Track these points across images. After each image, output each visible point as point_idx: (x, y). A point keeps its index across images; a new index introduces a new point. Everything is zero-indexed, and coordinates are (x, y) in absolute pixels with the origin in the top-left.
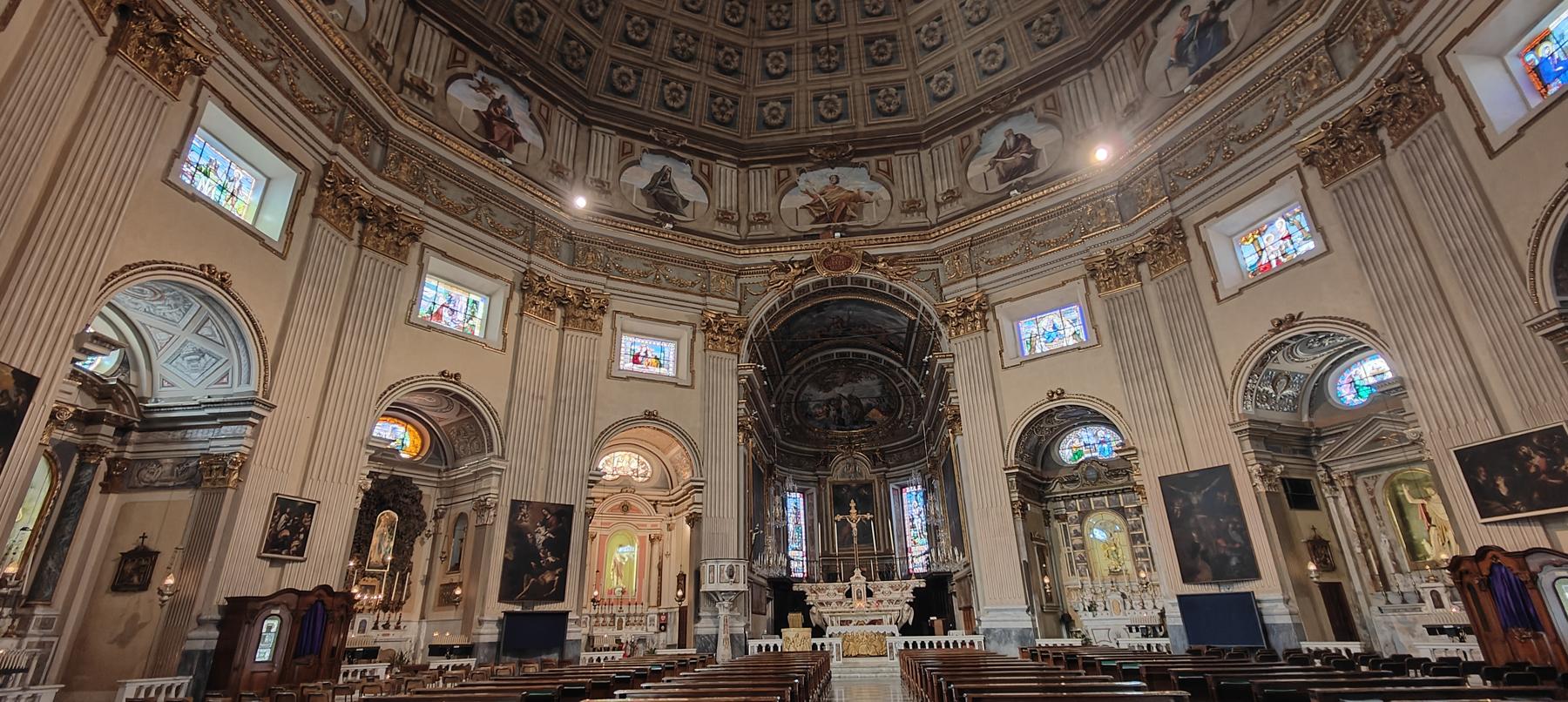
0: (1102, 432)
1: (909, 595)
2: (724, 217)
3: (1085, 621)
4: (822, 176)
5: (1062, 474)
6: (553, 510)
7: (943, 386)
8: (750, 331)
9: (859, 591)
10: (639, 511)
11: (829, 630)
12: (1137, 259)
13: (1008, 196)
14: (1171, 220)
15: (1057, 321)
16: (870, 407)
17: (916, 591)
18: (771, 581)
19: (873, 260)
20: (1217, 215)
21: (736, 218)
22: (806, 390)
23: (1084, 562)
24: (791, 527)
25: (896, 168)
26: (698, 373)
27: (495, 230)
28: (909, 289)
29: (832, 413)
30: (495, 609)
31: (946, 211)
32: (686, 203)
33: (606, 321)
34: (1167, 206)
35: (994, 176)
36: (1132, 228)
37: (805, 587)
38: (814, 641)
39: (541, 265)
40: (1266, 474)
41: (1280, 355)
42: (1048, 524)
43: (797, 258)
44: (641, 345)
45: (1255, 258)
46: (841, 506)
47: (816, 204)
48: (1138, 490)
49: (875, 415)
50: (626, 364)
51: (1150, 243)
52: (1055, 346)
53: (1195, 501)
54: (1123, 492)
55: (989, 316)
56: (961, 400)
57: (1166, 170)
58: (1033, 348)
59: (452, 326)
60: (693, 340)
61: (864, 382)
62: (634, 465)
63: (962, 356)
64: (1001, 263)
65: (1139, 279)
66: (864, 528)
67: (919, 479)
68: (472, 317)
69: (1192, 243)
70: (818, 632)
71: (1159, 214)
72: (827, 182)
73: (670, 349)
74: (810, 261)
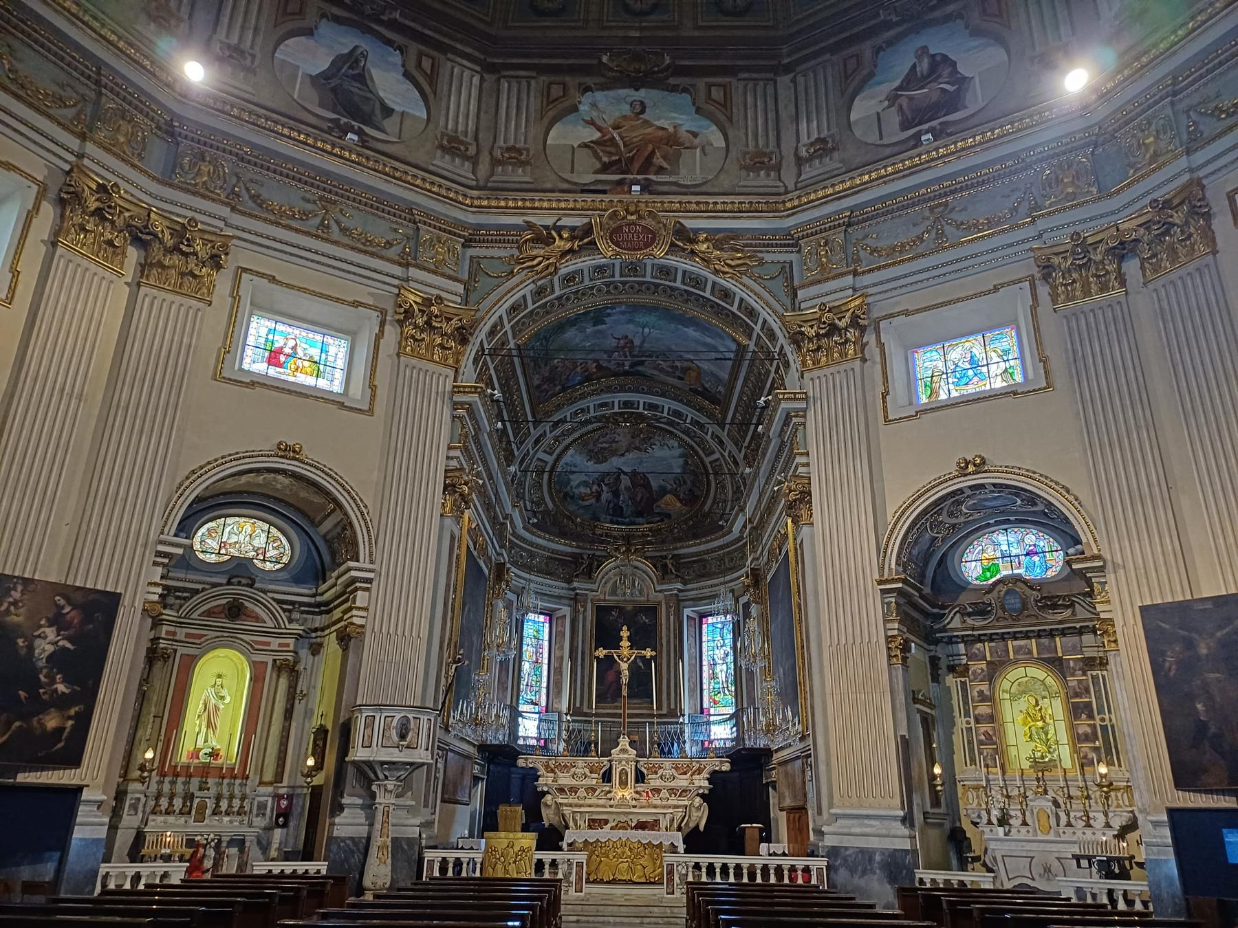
0: (1032, 538)
1: (702, 783)
2: (452, 146)
3: (989, 838)
4: (619, 100)
5: (964, 599)
7: (788, 450)
8: (481, 334)
9: (623, 773)
10: (257, 618)
11: (569, 836)
12: (1122, 250)
13: (918, 143)
14: (1190, 183)
15: (978, 351)
16: (663, 491)
17: (714, 777)
18: (483, 748)
21: (472, 151)
22: (567, 458)
23: (992, 745)
24: (526, 667)
25: (737, 99)
26: (382, 394)
28: (744, 290)
32: (388, 111)
33: (222, 282)
36: (1116, 203)
37: (536, 761)
38: (539, 855)
39: (102, 164)
42: (936, 678)
44: (286, 335)
47: (605, 143)
48: (1101, 628)
49: (670, 503)
50: (254, 363)
51: (1146, 225)
54: (1063, 633)
55: (870, 338)
56: (814, 469)
57: (1181, 106)
60: (379, 336)
61: (658, 452)
62: (260, 541)
63: (819, 399)
64: (895, 255)
65: (1123, 283)
66: (640, 676)
67: (729, 603)
70: (550, 838)
71: (1169, 178)
72: (626, 110)
73: (338, 350)
74: (588, 230)
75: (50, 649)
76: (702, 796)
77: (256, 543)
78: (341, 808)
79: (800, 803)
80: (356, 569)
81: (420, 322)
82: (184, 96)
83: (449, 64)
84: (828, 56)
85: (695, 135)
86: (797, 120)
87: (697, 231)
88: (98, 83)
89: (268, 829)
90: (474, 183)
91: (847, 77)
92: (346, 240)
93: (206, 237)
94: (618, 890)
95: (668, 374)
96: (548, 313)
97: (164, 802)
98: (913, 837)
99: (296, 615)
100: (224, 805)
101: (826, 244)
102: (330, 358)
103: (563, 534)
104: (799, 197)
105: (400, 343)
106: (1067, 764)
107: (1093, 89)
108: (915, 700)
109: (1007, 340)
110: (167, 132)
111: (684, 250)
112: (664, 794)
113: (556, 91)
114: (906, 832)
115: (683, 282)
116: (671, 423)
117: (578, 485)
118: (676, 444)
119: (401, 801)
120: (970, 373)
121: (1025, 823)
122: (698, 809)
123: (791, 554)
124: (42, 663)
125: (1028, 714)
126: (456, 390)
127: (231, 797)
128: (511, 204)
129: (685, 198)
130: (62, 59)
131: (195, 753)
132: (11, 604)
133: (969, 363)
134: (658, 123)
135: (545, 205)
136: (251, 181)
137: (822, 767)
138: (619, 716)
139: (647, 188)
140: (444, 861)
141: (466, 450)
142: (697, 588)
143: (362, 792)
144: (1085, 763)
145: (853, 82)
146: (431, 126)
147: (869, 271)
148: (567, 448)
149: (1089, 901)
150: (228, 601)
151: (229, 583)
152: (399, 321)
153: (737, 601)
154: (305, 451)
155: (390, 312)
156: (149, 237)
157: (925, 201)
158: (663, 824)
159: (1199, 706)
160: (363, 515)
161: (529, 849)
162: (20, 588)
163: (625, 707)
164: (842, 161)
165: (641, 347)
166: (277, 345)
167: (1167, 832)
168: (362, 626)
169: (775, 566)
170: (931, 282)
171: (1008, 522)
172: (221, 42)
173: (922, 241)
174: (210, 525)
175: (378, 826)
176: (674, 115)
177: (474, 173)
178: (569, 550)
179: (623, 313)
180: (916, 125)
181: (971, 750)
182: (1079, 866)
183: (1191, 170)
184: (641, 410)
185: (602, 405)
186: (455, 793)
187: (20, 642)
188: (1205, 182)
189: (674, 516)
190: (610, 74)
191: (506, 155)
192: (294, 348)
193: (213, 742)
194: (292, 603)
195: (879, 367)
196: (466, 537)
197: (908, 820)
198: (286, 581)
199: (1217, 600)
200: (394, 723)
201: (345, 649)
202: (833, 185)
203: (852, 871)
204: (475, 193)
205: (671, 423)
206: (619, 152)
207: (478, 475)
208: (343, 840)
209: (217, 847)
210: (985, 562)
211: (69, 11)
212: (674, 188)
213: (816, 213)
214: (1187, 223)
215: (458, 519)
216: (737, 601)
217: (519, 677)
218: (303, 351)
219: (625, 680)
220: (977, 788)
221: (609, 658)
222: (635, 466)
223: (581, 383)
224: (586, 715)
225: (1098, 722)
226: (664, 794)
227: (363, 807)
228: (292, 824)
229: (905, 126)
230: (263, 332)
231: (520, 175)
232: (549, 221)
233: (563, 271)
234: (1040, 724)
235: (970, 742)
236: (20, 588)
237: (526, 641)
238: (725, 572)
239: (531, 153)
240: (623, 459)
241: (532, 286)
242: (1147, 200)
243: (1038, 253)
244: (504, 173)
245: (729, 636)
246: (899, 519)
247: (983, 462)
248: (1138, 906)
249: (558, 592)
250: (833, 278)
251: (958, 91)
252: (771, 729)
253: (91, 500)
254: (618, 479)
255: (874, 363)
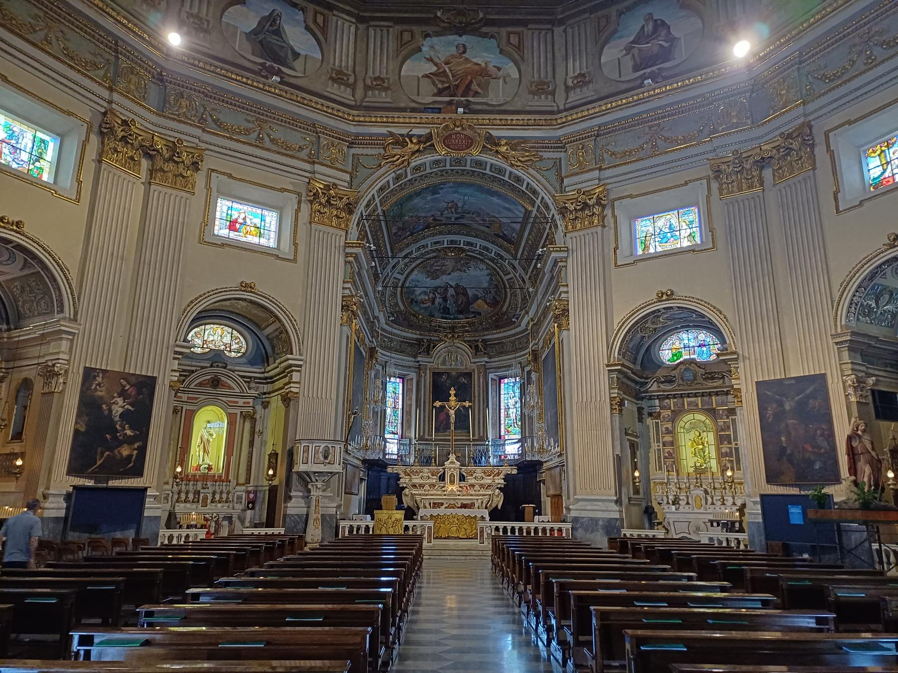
0: (703, 336)
1: (500, 481)
2: (338, 77)
5: (660, 373)
6: (133, 380)
7: (556, 282)
8: (361, 208)
9: (452, 475)
10: (230, 387)
11: (422, 512)
12: (763, 163)
13: (641, 85)
14: (803, 123)
15: (674, 221)
16: (476, 298)
17: (507, 478)
18: (364, 461)
19: (493, 142)
20: (850, 123)
21: (352, 80)
22: (413, 276)
23: (672, 459)
24: (389, 411)
25: (527, 43)
27: (70, 58)
28: (529, 177)
29: (438, 300)
30: (60, 483)
31: (575, 97)
32: (296, 55)
33: (200, 179)
34: (801, 110)
35: (628, 63)
40: (859, 384)
41: (888, 271)
42: (641, 420)
43: (416, 131)
44: (240, 211)
45: (879, 171)
46: (439, 392)
49: (480, 306)
50: (221, 230)
51: (777, 148)
52: (669, 247)
53: (787, 407)
54: (717, 394)
55: (608, 212)
56: (571, 295)
58: (646, 247)
59: (14, 166)
60: (298, 211)
61: (472, 272)
62: (227, 339)
63: (576, 249)
65: (762, 184)
66: (462, 417)
67: (519, 371)
68: (40, 158)
69: (820, 151)
70: (410, 514)
71: (790, 120)
72: (453, 50)
73: (271, 218)
74: (429, 137)
75: (121, 410)
76: (500, 489)
77: (224, 340)
78: (290, 498)
79: (558, 493)
80: (293, 359)
81: (323, 201)
82: (167, 53)
83: (334, 18)
84: (587, 15)
85: (499, 69)
86: (566, 58)
87: (500, 138)
88: (116, 51)
89: (244, 510)
90: (353, 103)
91: (600, 32)
92: (274, 148)
93: (188, 150)
94: (451, 543)
95: (480, 224)
96: (402, 189)
97: (183, 496)
98: (621, 512)
99: (253, 385)
100: (217, 497)
101: (582, 148)
102: (267, 225)
103: (411, 326)
104: (566, 116)
105: (311, 215)
106: (714, 469)
107: (754, 54)
108: (627, 434)
109: (692, 215)
110: (158, 79)
111: (491, 150)
112: (477, 487)
113: (407, 36)
114: (617, 508)
115: (491, 170)
116: (481, 254)
117: (420, 294)
118: (485, 267)
119: (325, 494)
120: (669, 235)
121: (688, 503)
122: (497, 496)
123: (556, 345)
124: (117, 419)
125: (694, 442)
126: (347, 245)
127: (221, 493)
128: (379, 119)
129: (492, 116)
130: (93, 37)
131: (198, 468)
132: (97, 385)
133: (670, 229)
134: (474, 60)
135: (401, 120)
136: (213, 110)
137: (571, 472)
138: (449, 440)
139: (467, 106)
140: (351, 527)
141: (354, 282)
142: (496, 361)
143: (302, 489)
144: (724, 470)
145: (603, 36)
146: (324, 63)
147: (609, 168)
148: (412, 270)
149: (724, 544)
150: (207, 377)
151: (211, 366)
152: (309, 201)
153: (523, 370)
154: (257, 287)
155: (304, 194)
156: (154, 153)
157: (645, 122)
158: (476, 506)
159: (783, 439)
160: (293, 326)
161: (400, 519)
162: (101, 375)
163: (452, 434)
164: (595, 91)
165: (463, 207)
166: (234, 217)
167: (759, 507)
168: (297, 393)
169: (547, 351)
170: (648, 177)
171: (688, 326)
172: (187, 12)
173: (643, 149)
174: (196, 330)
175: (313, 508)
176: (485, 54)
177: (353, 96)
178: (415, 336)
179: (451, 187)
180: (644, 69)
181: (660, 462)
182: (712, 526)
183: (805, 115)
184: (462, 245)
185: (436, 243)
186: (351, 489)
187: (104, 406)
188: (812, 123)
189: (483, 314)
190: (442, 25)
191: (375, 83)
192: (244, 219)
193: (207, 461)
194: (250, 377)
195: (613, 231)
196: (354, 336)
197: (618, 502)
198: (245, 364)
199: (798, 379)
200: (321, 450)
201: (287, 406)
202: (588, 110)
203: (586, 530)
204: (355, 112)
205: (481, 254)
206: (449, 81)
207: (361, 297)
208: (293, 515)
209: (217, 522)
210: (674, 351)
211: (97, 6)
212: (485, 107)
213: (577, 127)
214: (800, 149)
215: (350, 326)
216: (523, 370)
217: (385, 417)
218: (251, 222)
219: (452, 420)
220: (662, 484)
221: (442, 407)
222: (457, 286)
223: (423, 230)
224: (427, 440)
225: (734, 446)
226: (477, 487)
227: (303, 497)
228: (257, 508)
229: (636, 68)
230: (225, 209)
231: (383, 98)
232: (404, 131)
233: (413, 164)
234: (701, 447)
235: (659, 457)
236: (101, 375)
237: (389, 395)
238: (516, 350)
239: (391, 81)
240: (449, 277)
241: (393, 175)
242: (778, 132)
243: (713, 162)
244: (374, 95)
245: (518, 391)
246: (621, 327)
247: (672, 294)
248: (742, 547)
249: (408, 364)
250: (587, 172)
251: (671, 46)
252: (542, 450)
253: (134, 321)
254: (446, 289)
255: (610, 228)
